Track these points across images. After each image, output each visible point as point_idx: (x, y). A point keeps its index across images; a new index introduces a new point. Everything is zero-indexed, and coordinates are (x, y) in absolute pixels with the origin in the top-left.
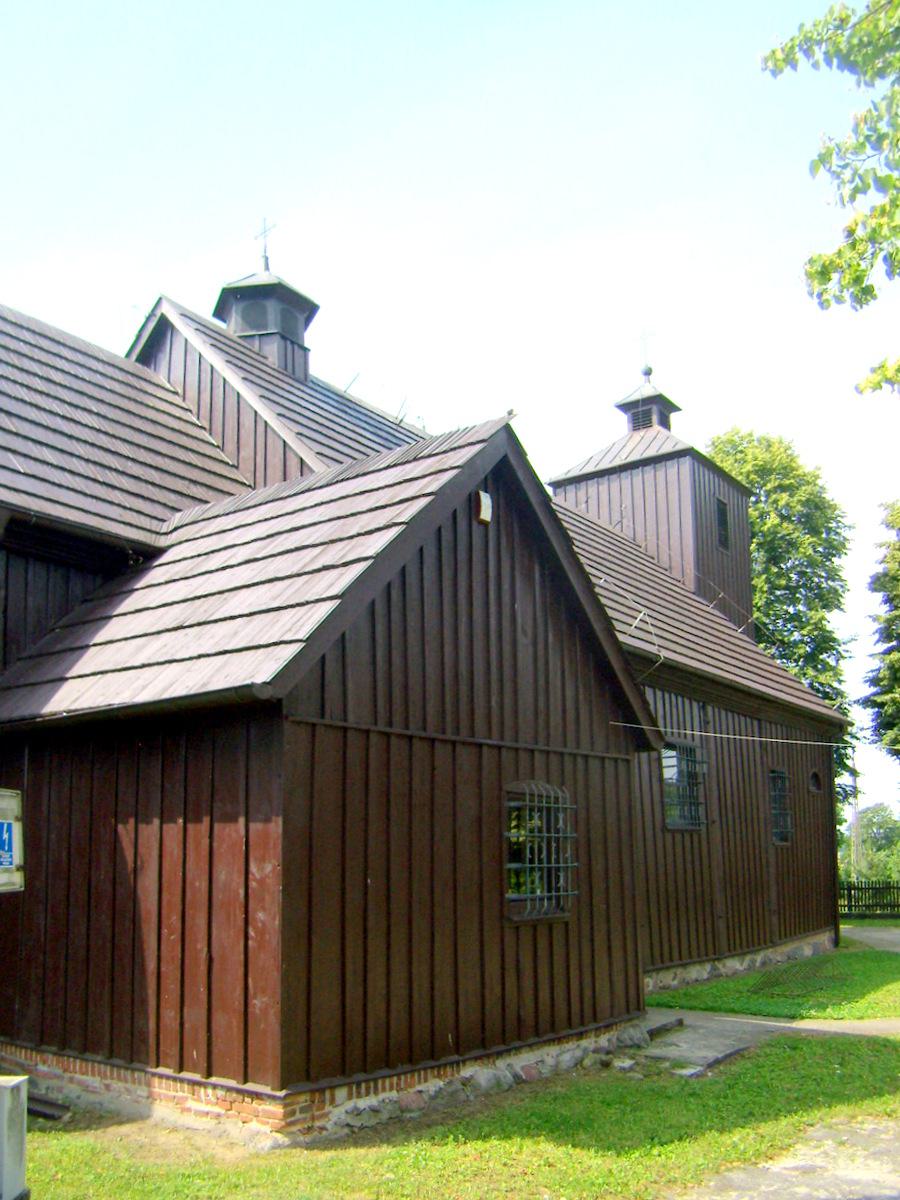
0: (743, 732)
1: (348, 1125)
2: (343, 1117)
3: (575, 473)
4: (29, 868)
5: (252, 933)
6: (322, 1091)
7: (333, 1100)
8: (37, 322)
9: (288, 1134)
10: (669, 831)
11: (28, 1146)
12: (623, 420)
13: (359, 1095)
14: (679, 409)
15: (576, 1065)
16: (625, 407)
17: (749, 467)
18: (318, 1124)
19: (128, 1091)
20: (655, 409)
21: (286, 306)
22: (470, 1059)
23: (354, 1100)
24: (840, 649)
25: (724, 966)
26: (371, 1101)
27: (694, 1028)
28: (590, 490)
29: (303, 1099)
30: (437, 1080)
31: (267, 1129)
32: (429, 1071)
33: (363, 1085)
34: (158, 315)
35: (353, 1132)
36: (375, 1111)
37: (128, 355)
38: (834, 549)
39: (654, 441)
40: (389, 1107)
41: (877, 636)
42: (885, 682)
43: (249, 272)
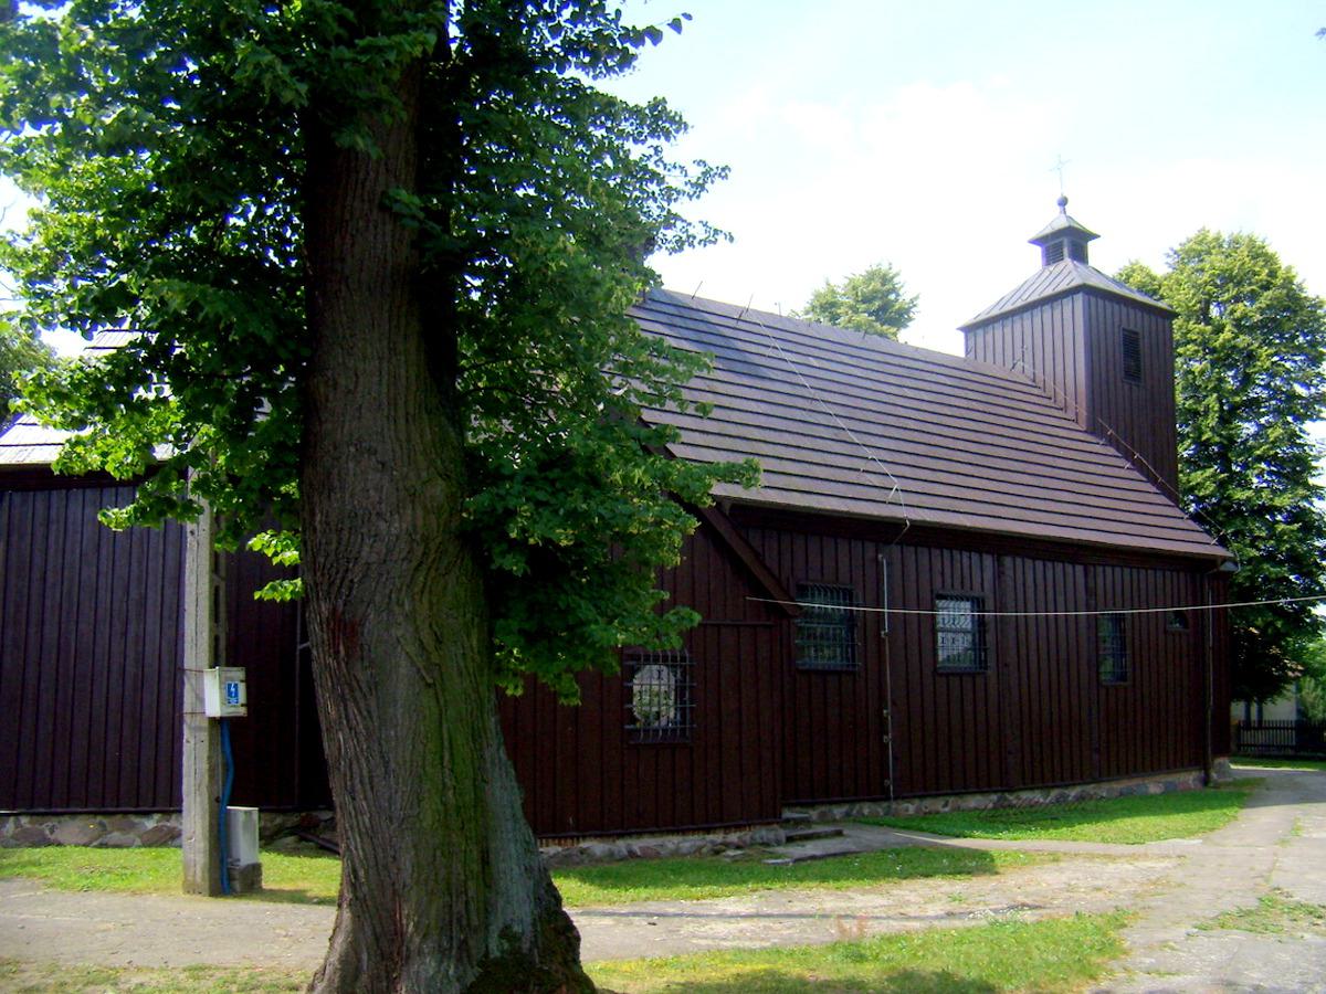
4: (247, 705)
10: (941, 675)
11: (1272, 718)
16: (1036, 242)
17: (1206, 277)
22: (590, 836)
27: (849, 836)
28: (1045, 316)
39: (1068, 274)
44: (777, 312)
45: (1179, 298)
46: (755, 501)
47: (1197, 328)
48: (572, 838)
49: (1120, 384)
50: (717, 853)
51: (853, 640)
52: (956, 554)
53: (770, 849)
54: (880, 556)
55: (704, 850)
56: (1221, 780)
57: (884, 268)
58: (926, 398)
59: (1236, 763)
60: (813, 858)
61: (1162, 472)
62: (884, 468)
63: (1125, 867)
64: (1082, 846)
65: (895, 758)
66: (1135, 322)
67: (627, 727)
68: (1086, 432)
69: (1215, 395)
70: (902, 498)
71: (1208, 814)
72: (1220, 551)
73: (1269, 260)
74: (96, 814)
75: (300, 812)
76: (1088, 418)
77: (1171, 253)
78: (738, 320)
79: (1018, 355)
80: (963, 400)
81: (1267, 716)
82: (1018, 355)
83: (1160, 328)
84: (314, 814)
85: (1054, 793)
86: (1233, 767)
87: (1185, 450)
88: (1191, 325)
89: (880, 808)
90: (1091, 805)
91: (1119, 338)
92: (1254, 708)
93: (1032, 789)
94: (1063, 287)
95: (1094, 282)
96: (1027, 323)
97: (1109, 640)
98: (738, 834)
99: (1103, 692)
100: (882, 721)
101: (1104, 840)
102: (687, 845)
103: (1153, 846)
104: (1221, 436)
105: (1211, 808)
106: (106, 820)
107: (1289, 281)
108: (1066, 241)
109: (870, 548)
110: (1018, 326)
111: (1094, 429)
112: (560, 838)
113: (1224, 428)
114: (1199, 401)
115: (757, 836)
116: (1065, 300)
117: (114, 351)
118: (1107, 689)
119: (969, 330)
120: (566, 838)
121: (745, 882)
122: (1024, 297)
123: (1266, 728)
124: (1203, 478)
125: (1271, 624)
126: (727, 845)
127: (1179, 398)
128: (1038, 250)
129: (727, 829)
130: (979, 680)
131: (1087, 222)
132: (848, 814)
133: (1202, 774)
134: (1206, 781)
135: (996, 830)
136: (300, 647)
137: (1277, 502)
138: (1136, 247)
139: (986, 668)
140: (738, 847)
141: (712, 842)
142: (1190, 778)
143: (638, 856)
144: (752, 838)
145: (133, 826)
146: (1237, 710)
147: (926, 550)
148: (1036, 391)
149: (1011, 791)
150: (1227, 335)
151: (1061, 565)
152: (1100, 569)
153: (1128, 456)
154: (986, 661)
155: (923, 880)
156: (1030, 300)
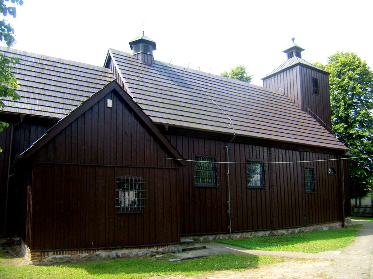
0: (311, 158)
1: (52, 261)
2: (50, 259)
3: (269, 75)
6: (45, 252)
7: (48, 255)
9: (33, 262)
10: (249, 189)
12: (285, 55)
13: (57, 254)
14: (305, 50)
15: (145, 255)
16: (285, 52)
17: (339, 64)
18: (43, 260)
21: (145, 44)
22: (100, 249)
23: (55, 255)
25: (277, 232)
26: (61, 256)
27: (208, 249)
29: (38, 253)
30: (87, 253)
32: (83, 251)
33: (58, 252)
35: (53, 263)
36: (61, 258)
37: (104, 67)
39: (295, 60)
40: (67, 258)
43: (137, 36)
44: (198, 70)
45: (331, 70)
46: (178, 126)
47: (336, 80)
48: (93, 250)
49: (312, 95)
50: (152, 256)
51: (216, 176)
52: (254, 147)
53: (174, 255)
54: (226, 147)
55: (148, 255)
56: (348, 225)
57: (242, 66)
58: (247, 97)
59: (352, 218)
60: (189, 258)
61: (327, 124)
62: (228, 117)
63: (307, 266)
64: (295, 254)
65: (232, 219)
66: (316, 75)
67: (116, 207)
68: (301, 110)
69: (343, 101)
70: (233, 126)
71: (343, 239)
72: (345, 148)
73: (358, 59)
75: (7, 238)
76: (302, 105)
77: (328, 58)
78: (184, 71)
79: (279, 86)
80: (266, 102)
81: (362, 204)
82: (279, 86)
83: (325, 78)
84: (13, 238)
85: (290, 231)
86: (352, 220)
87: (334, 118)
88: (335, 78)
89: (227, 237)
90: (302, 235)
91: (311, 81)
92: (358, 201)
93: (282, 229)
94: (293, 64)
95: (303, 62)
96: (282, 76)
97: (308, 178)
98: (163, 248)
99: (307, 195)
100: (227, 205)
101: (303, 251)
102: (141, 253)
103: (322, 255)
104: (345, 114)
105: (345, 236)
107: (365, 65)
108: (294, 51)
109: (222, 144)
110: (279, 77)
111: (304, 109)
112: (88, 250)
113: (346, 111)
114: (338, 103)
115: (170, 249)
116: (293, 68)
118: (308, 194)
119: (264, 79)
120: (90, 250)
121: (150, 271)
122: (281, 68)
123: (362, 207)
124: (340, 127)
125: (363, 173)
126: (158, 253)
127: (331, 102)
128: (286, 55)
129: (158, 246)
130: (263, 191)
132: (214, 239)
133: (342, 223)
134: (343, 226)
135: (265, 246)
136: (9, 176)
137: (364, 134)
138: (317, 56)
139: (265, 187)
140: (163, 253)
141: (152, 252)
142: (337, 225)
143: (120, 257)
144: (168, 250)
146: (353, 201)
147: (247, 146)
148: (285, 97)
149: (275, 230)
150: (346, 81)
151: (291, 151)
152: (305, 153)
153: (315, 118)
154: (265, 184)
155: (225, 271)
156: (283, 69)
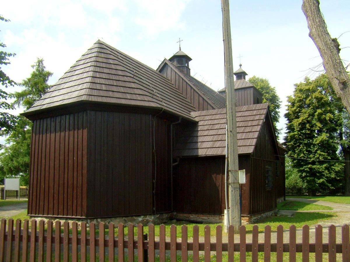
5: (243, 191)
8: (138, 61)
19: (214, 219)
20: (243, 75)
24: (279, 132)
31: (245, 221)
34: (164, 63)
37: (157, 70)
38: (278, 107)
41: (286, 128)
42: (289, 140)
74: (123, 217)
106: (126, 219)
117: (235, 85)
131: (186, 51)
145: (134, 220)
